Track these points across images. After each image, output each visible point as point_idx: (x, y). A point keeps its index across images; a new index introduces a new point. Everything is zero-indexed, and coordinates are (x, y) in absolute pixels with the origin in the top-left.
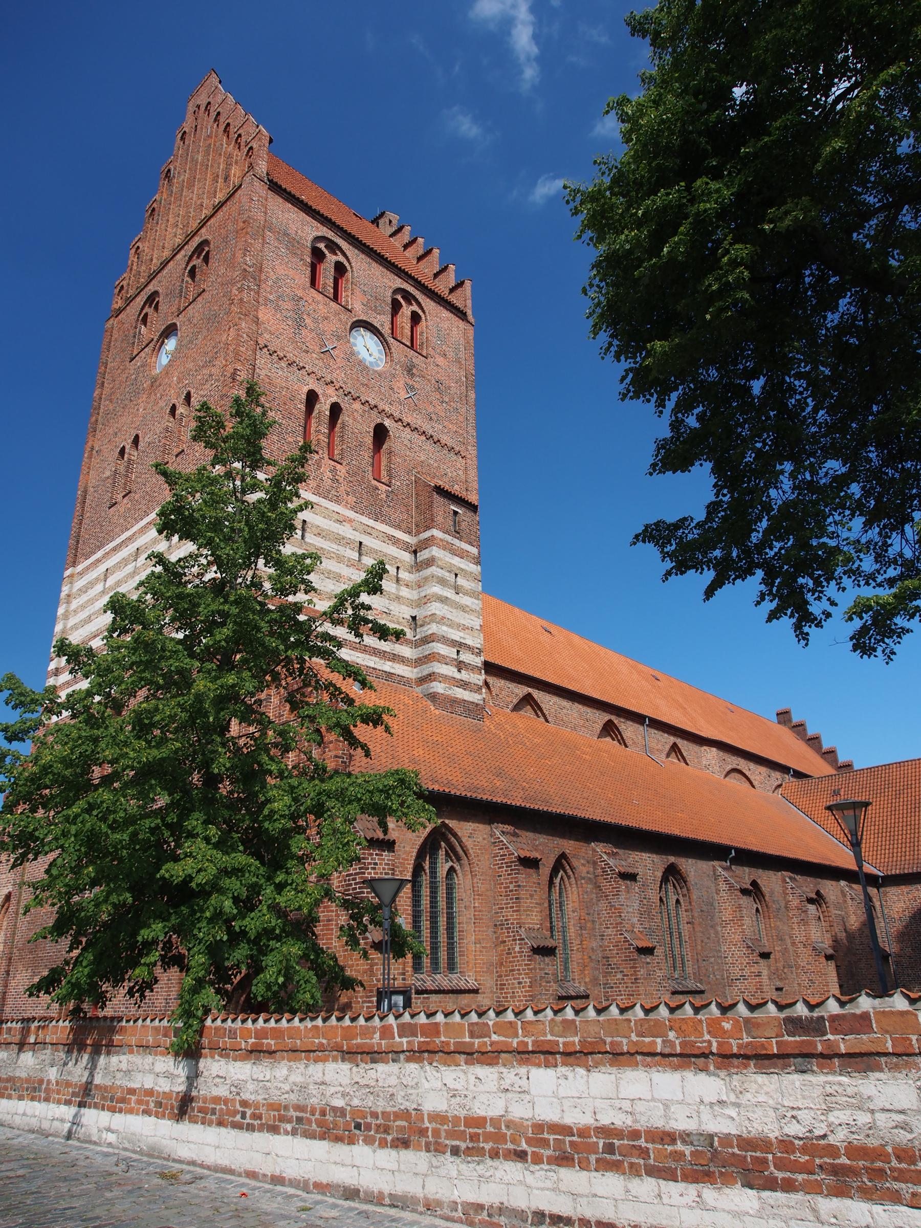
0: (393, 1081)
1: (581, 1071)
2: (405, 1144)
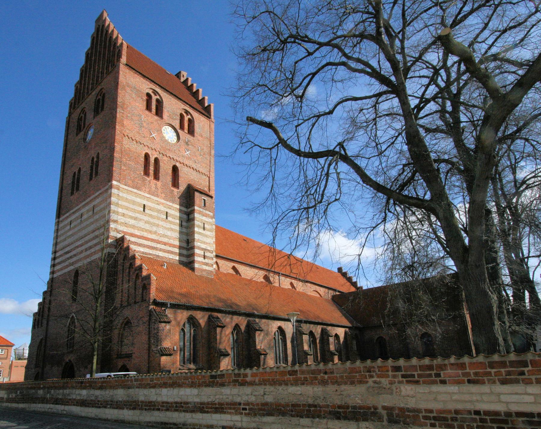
0: (133, 393)
1: (172, 389)
2: (134, 409)
